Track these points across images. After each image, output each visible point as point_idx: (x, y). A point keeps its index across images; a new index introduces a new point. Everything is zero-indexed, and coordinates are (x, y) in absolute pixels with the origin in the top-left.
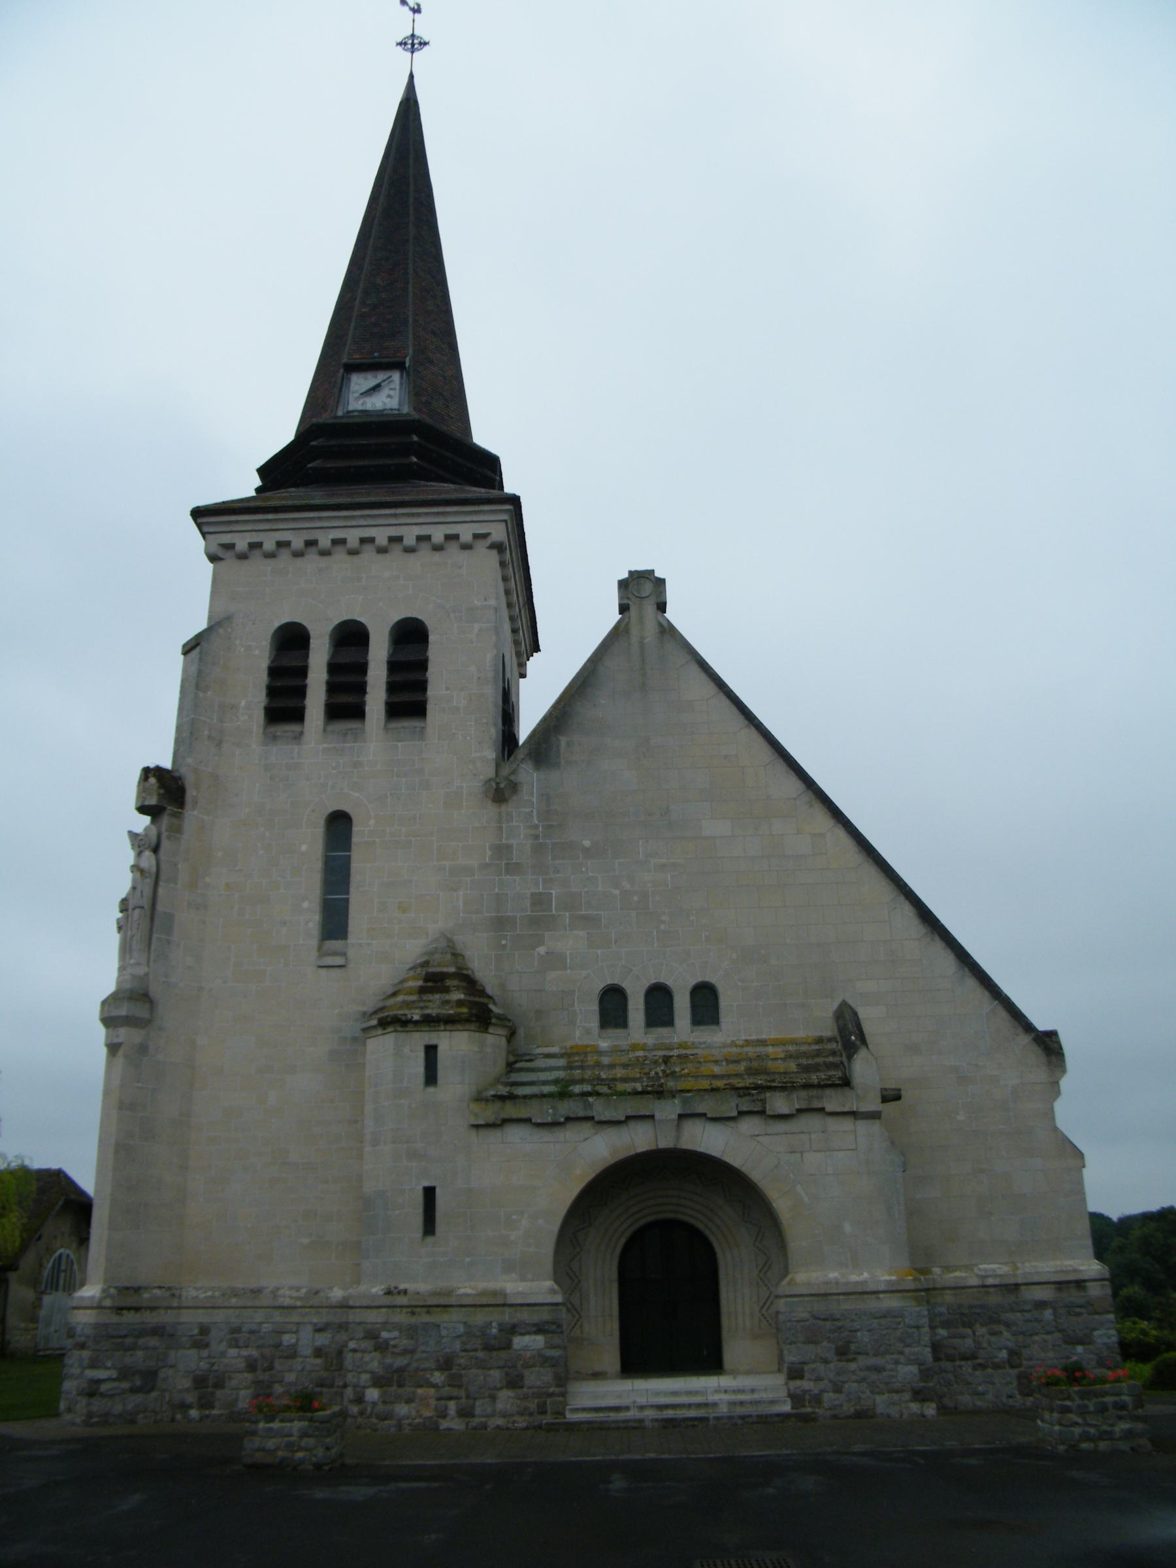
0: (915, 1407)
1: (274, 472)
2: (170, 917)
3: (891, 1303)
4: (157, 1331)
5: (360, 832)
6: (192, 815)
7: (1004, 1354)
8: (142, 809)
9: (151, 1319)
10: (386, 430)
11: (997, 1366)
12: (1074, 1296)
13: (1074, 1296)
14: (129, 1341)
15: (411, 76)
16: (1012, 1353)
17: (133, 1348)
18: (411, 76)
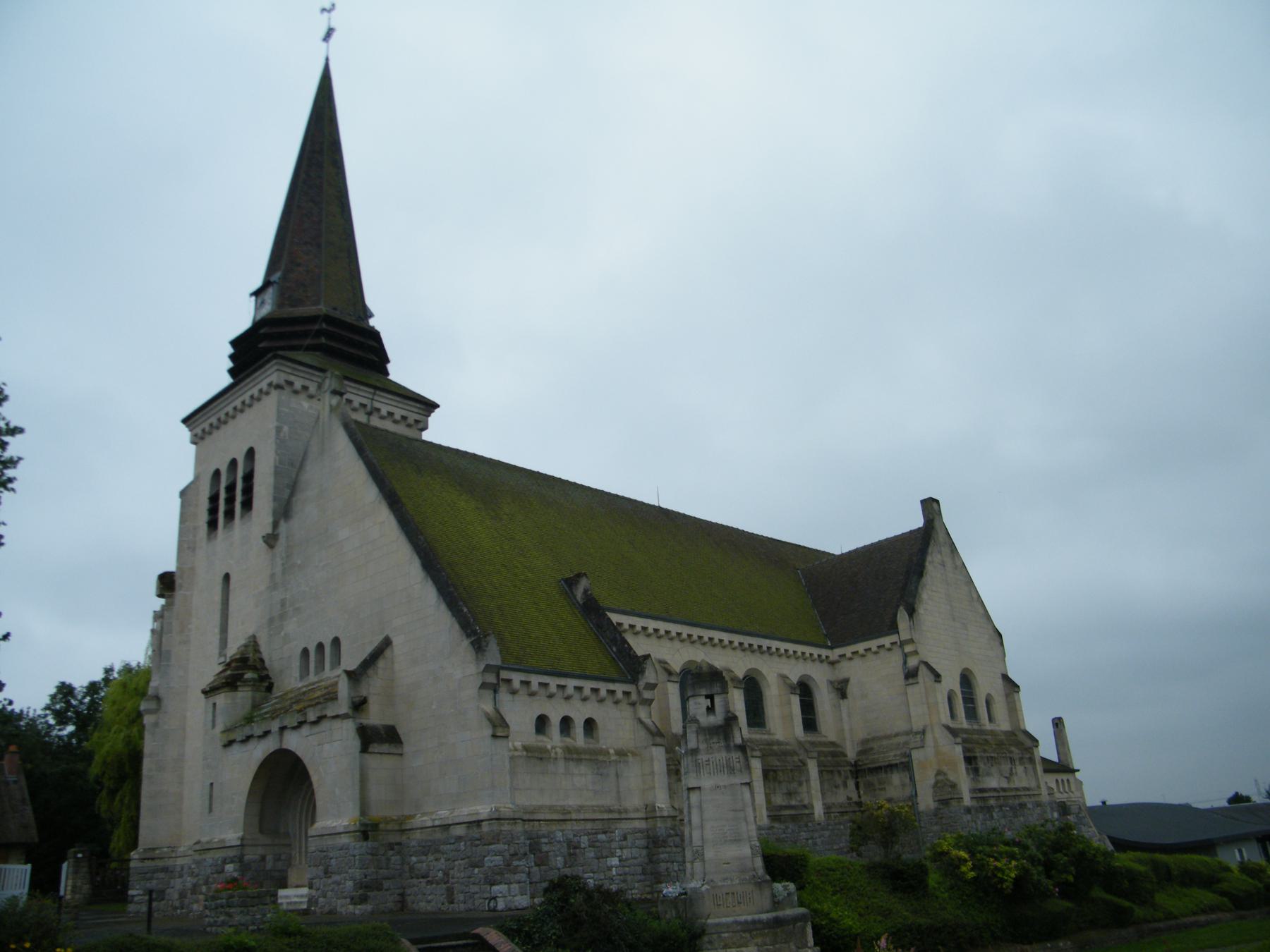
0: (351, 907)
1: (232, 372)
2: (169, 652)
3: (345, 840)
4: (165, 870)
5: (233, 581)
6: (179, 594)
7: (440, 874)
8: (160, 596)
9: (160, 863)
10: (312, 318)
11: (438, 883)
12: (475, 832)
13: (475, 832)
14: (148, 875)
15: (327, 59)
16: (446, 874)
17: (151, 879)
18: (327, 59)
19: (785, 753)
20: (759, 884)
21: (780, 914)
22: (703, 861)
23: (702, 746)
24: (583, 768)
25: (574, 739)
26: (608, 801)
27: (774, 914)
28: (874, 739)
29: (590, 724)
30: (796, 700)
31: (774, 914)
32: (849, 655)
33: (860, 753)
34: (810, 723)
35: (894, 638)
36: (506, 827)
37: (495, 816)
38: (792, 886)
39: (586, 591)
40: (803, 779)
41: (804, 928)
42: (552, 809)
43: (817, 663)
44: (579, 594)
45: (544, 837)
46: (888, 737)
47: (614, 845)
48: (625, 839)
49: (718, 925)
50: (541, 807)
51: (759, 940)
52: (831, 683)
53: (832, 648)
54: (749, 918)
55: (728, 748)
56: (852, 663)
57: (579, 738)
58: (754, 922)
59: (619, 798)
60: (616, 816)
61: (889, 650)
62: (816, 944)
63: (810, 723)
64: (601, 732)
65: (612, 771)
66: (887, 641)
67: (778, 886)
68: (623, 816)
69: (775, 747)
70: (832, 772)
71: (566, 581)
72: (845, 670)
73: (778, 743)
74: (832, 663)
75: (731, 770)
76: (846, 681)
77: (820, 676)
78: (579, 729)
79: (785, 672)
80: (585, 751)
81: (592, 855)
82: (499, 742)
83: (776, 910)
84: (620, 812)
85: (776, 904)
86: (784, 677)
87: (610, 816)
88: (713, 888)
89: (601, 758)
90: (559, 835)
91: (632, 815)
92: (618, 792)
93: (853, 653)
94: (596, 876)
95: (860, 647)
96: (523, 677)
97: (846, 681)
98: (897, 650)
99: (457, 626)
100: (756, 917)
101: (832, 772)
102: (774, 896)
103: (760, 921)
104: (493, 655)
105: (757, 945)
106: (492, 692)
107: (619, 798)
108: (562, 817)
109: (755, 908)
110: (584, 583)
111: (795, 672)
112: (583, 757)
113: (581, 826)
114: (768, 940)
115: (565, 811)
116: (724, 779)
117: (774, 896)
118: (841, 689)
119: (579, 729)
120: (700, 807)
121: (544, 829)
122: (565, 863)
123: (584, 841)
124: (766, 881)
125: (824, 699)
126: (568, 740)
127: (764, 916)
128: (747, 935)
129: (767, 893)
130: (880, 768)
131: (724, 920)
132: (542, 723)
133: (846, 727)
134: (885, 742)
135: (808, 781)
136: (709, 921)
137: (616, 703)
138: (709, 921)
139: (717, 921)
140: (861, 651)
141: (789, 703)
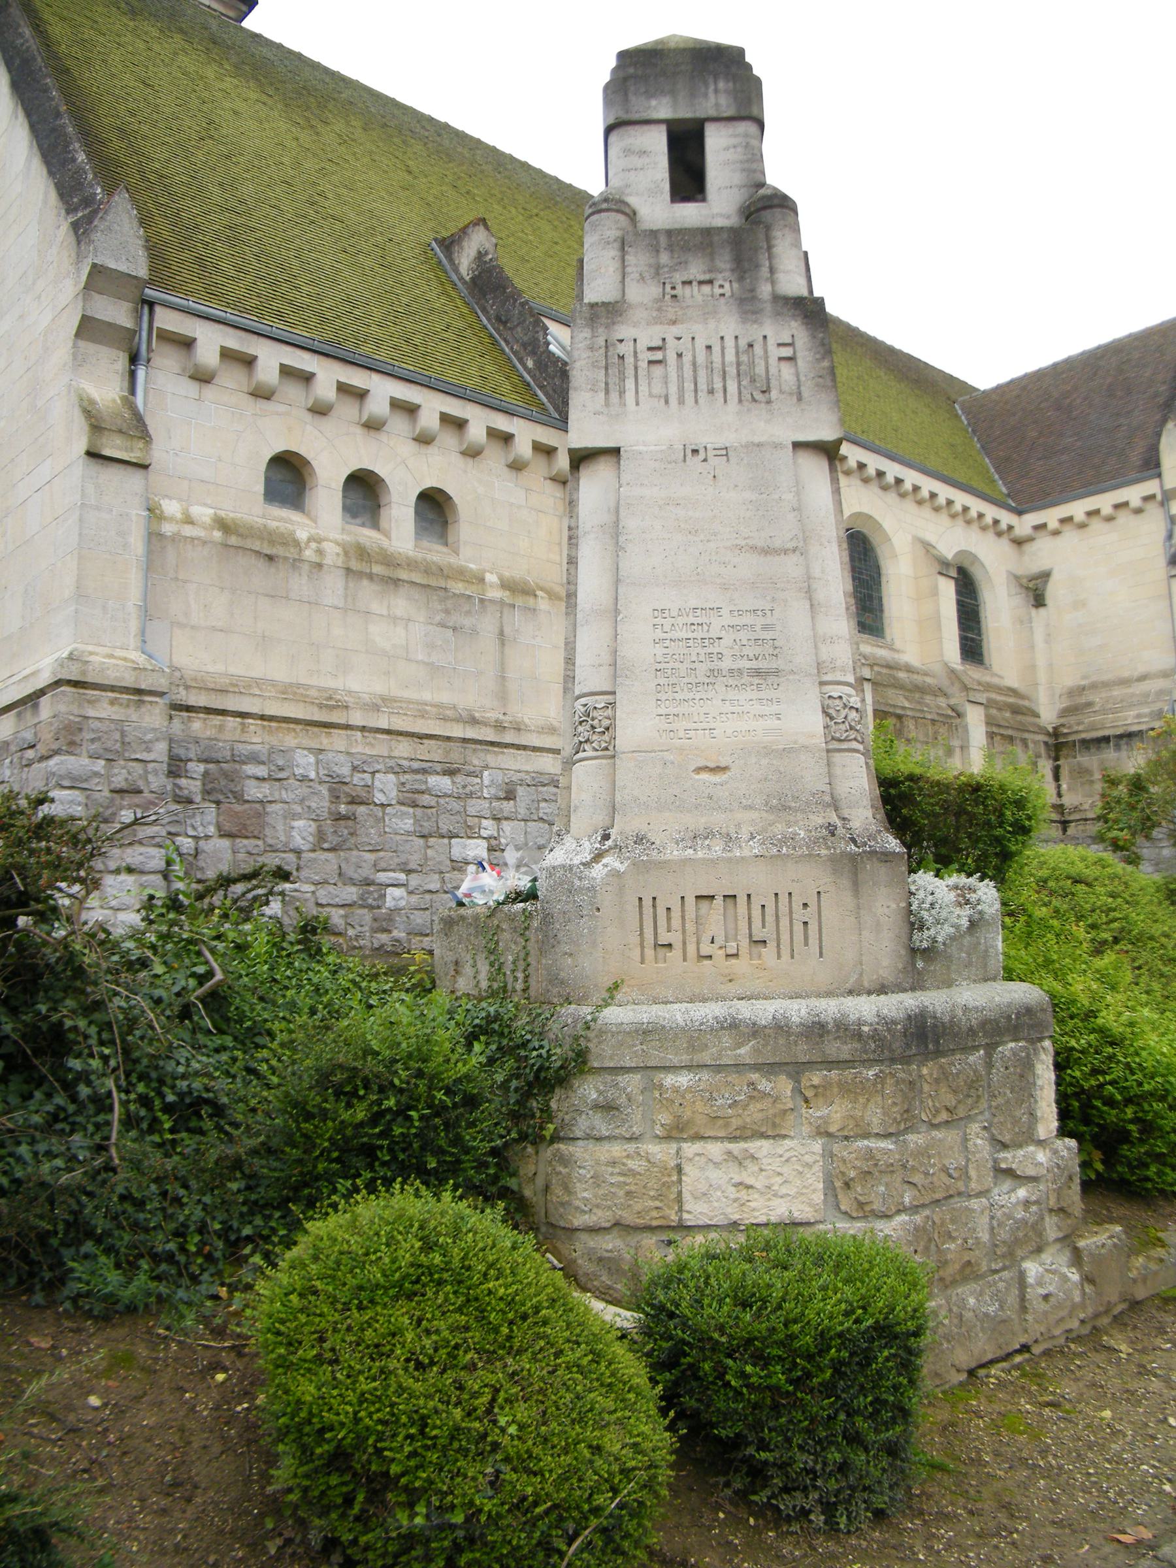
19: (922, 690)
20: (853, 865)
21: (933, 1001)
22: (609, 752)
23: (641, 293)
24: (401, 604)
25: (387, 535)
26: (474, 696)
27: (909, 1001)
28: (1094, 686)
29: (434, 506)
30: (948, 590)
31: (909, 1001)
32: (1053, 524)
33: (1065, 712)
34: (972, 650)
35: (1151, 487)
36: (104, 709)
37: (74, 674)
38: (987, 893)
39: (480, 255)
40: (956, 743)
41: (1027, 1065)
42: (289, 691)
43: (990, 535)
44: (465, 261)
45: (254, 759)
46: (1125, 682)
47: (474, 807)
48: (510, 796)
49: (646, 1032)
50: (258, 682)
51: (836, 1112)
52: (1017, 578)
53: (1020, 513)
54: (798, 1011)
55: (747, 305)
56: (1058, 540)
57: (400, 525)
58: (816, 1030)
59: (502, 696)
60: (489, 735)
61: (1138, 511)
62: (1063, 1132)
63: (972, 650)
64: (465, 528)
65: (487, 624)
66: (1133, 494)
67: (937, 889)
68: (508, 738)
69: (902, 675)
70: (1011, 739)
71: (441, 242)
72: (1044, 554)
73: (909, 669)
74: (1019, 542)
75: (759, 391)
76: (1046, 576)
77: (996, 564)
78: (400, 511)
79: (930, 537)
80: (412, 564)
81: (408, 824)
82: (112, 476)
83: (917, 985)
84: (499, 727)
85: (921, 958)
86: (927, 546)
87: (471, 733)
88: (640, 867)
89: (458, 587)
90: (305, 763)
91: (535, 741)
92: (502, 678)
93: (1063, 521)
94: (414, 881)
95: (1078, 509)
96: (234, 341)
97: (1046, 576)
98: (1153, 509)
99: (53, 195)
100: (830, 1008)
101: (1011, 739)
102: (913, 923)
103: (845, 1029)
104: (123, 245)
105: (822, 1132)
106: (121, 362)
107: (502, 696)
108: (319, 716)
109: (835, 959)
110: (477, 240)
111: (952, 540)
112: (403, 575)
113: (381, 747)
114: (875, 1117)
115: (331, 702)
116: (723, 423)
117: (913, 923)
118: (1035, 591)
119: (400, 511)
120: (615, 531)
121: (257, 738)
122: (321, 836)
123: (386, 787)
124: (886, 857)
125: (1000, 607)
126: (367, 535)
127: (865, 1009)
128: (784, 1085)
129: (884, 906)
130: (1106, 739)
131: (677, 1014)
132: (288, 475)
133: (1041, 661)
134: (1117, 692)
135: (964, 748)
136: (613, 1015)
137: (517, 466)
138: (613, 1015)
139: (646, 1014)
140: (1080, 516)
141: (935, 592)
